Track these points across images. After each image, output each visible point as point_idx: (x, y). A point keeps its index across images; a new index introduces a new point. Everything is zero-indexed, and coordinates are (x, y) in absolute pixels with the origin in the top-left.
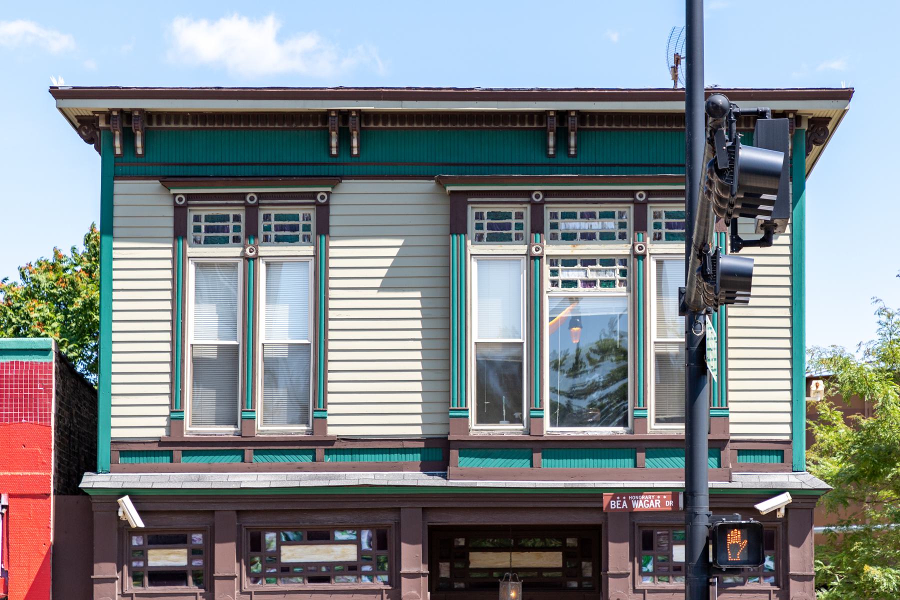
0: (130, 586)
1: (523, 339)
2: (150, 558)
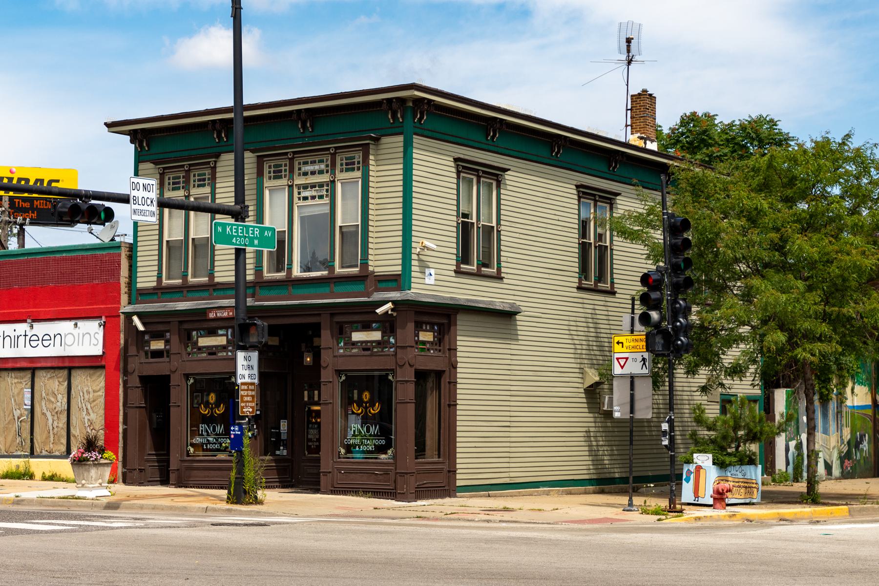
0: (143, 360)
1: (286, 229)
2: (151, 345)
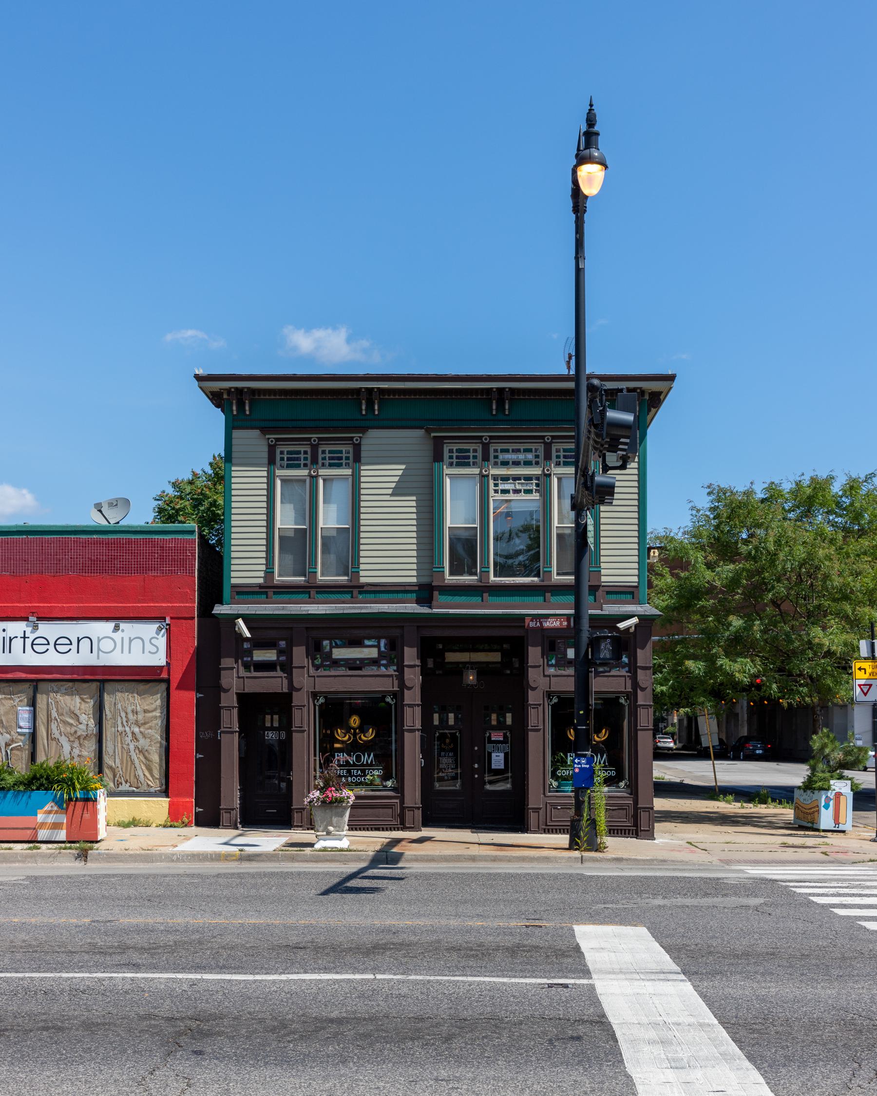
0: (242, 672)
2: (254, 655)
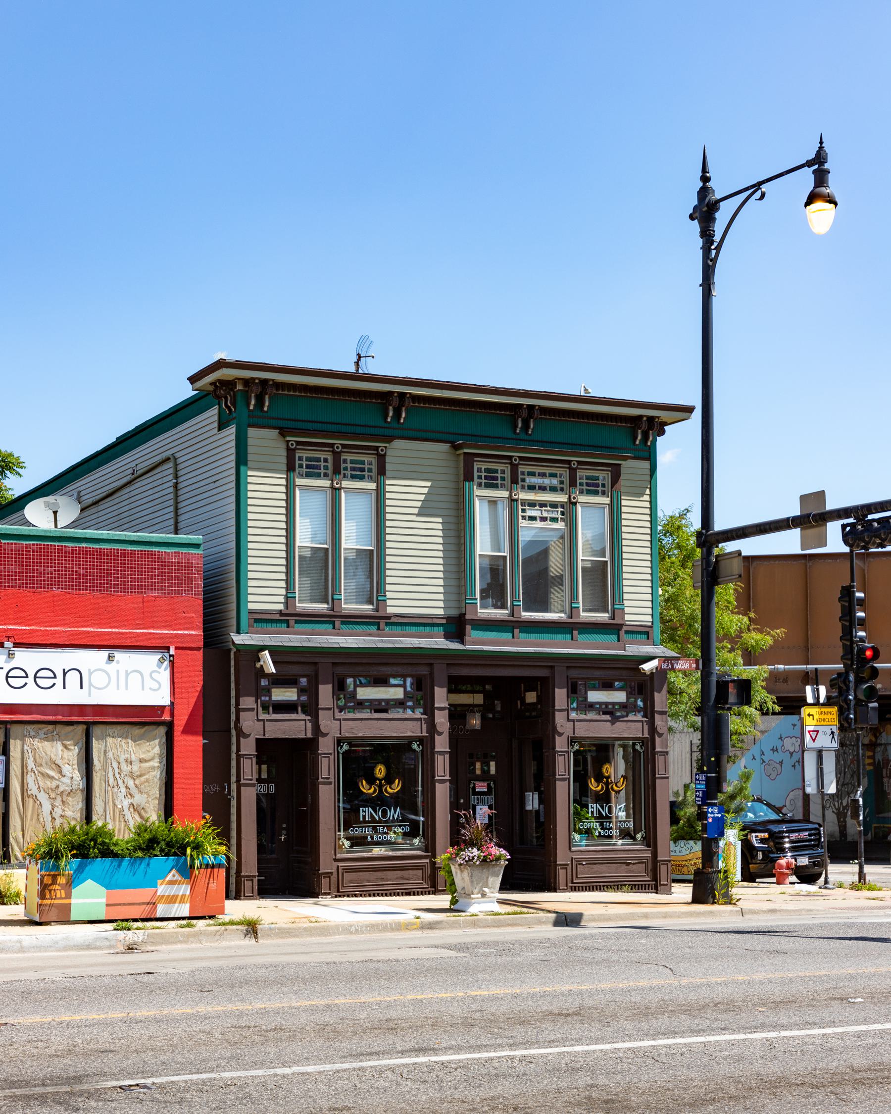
2: (273, 694)
